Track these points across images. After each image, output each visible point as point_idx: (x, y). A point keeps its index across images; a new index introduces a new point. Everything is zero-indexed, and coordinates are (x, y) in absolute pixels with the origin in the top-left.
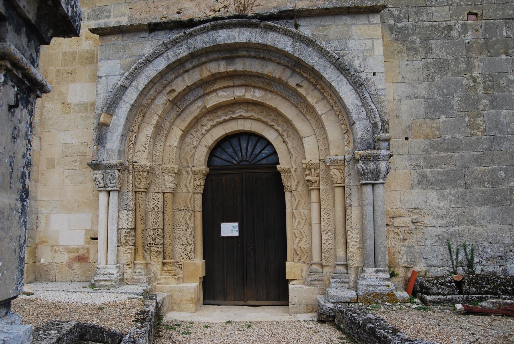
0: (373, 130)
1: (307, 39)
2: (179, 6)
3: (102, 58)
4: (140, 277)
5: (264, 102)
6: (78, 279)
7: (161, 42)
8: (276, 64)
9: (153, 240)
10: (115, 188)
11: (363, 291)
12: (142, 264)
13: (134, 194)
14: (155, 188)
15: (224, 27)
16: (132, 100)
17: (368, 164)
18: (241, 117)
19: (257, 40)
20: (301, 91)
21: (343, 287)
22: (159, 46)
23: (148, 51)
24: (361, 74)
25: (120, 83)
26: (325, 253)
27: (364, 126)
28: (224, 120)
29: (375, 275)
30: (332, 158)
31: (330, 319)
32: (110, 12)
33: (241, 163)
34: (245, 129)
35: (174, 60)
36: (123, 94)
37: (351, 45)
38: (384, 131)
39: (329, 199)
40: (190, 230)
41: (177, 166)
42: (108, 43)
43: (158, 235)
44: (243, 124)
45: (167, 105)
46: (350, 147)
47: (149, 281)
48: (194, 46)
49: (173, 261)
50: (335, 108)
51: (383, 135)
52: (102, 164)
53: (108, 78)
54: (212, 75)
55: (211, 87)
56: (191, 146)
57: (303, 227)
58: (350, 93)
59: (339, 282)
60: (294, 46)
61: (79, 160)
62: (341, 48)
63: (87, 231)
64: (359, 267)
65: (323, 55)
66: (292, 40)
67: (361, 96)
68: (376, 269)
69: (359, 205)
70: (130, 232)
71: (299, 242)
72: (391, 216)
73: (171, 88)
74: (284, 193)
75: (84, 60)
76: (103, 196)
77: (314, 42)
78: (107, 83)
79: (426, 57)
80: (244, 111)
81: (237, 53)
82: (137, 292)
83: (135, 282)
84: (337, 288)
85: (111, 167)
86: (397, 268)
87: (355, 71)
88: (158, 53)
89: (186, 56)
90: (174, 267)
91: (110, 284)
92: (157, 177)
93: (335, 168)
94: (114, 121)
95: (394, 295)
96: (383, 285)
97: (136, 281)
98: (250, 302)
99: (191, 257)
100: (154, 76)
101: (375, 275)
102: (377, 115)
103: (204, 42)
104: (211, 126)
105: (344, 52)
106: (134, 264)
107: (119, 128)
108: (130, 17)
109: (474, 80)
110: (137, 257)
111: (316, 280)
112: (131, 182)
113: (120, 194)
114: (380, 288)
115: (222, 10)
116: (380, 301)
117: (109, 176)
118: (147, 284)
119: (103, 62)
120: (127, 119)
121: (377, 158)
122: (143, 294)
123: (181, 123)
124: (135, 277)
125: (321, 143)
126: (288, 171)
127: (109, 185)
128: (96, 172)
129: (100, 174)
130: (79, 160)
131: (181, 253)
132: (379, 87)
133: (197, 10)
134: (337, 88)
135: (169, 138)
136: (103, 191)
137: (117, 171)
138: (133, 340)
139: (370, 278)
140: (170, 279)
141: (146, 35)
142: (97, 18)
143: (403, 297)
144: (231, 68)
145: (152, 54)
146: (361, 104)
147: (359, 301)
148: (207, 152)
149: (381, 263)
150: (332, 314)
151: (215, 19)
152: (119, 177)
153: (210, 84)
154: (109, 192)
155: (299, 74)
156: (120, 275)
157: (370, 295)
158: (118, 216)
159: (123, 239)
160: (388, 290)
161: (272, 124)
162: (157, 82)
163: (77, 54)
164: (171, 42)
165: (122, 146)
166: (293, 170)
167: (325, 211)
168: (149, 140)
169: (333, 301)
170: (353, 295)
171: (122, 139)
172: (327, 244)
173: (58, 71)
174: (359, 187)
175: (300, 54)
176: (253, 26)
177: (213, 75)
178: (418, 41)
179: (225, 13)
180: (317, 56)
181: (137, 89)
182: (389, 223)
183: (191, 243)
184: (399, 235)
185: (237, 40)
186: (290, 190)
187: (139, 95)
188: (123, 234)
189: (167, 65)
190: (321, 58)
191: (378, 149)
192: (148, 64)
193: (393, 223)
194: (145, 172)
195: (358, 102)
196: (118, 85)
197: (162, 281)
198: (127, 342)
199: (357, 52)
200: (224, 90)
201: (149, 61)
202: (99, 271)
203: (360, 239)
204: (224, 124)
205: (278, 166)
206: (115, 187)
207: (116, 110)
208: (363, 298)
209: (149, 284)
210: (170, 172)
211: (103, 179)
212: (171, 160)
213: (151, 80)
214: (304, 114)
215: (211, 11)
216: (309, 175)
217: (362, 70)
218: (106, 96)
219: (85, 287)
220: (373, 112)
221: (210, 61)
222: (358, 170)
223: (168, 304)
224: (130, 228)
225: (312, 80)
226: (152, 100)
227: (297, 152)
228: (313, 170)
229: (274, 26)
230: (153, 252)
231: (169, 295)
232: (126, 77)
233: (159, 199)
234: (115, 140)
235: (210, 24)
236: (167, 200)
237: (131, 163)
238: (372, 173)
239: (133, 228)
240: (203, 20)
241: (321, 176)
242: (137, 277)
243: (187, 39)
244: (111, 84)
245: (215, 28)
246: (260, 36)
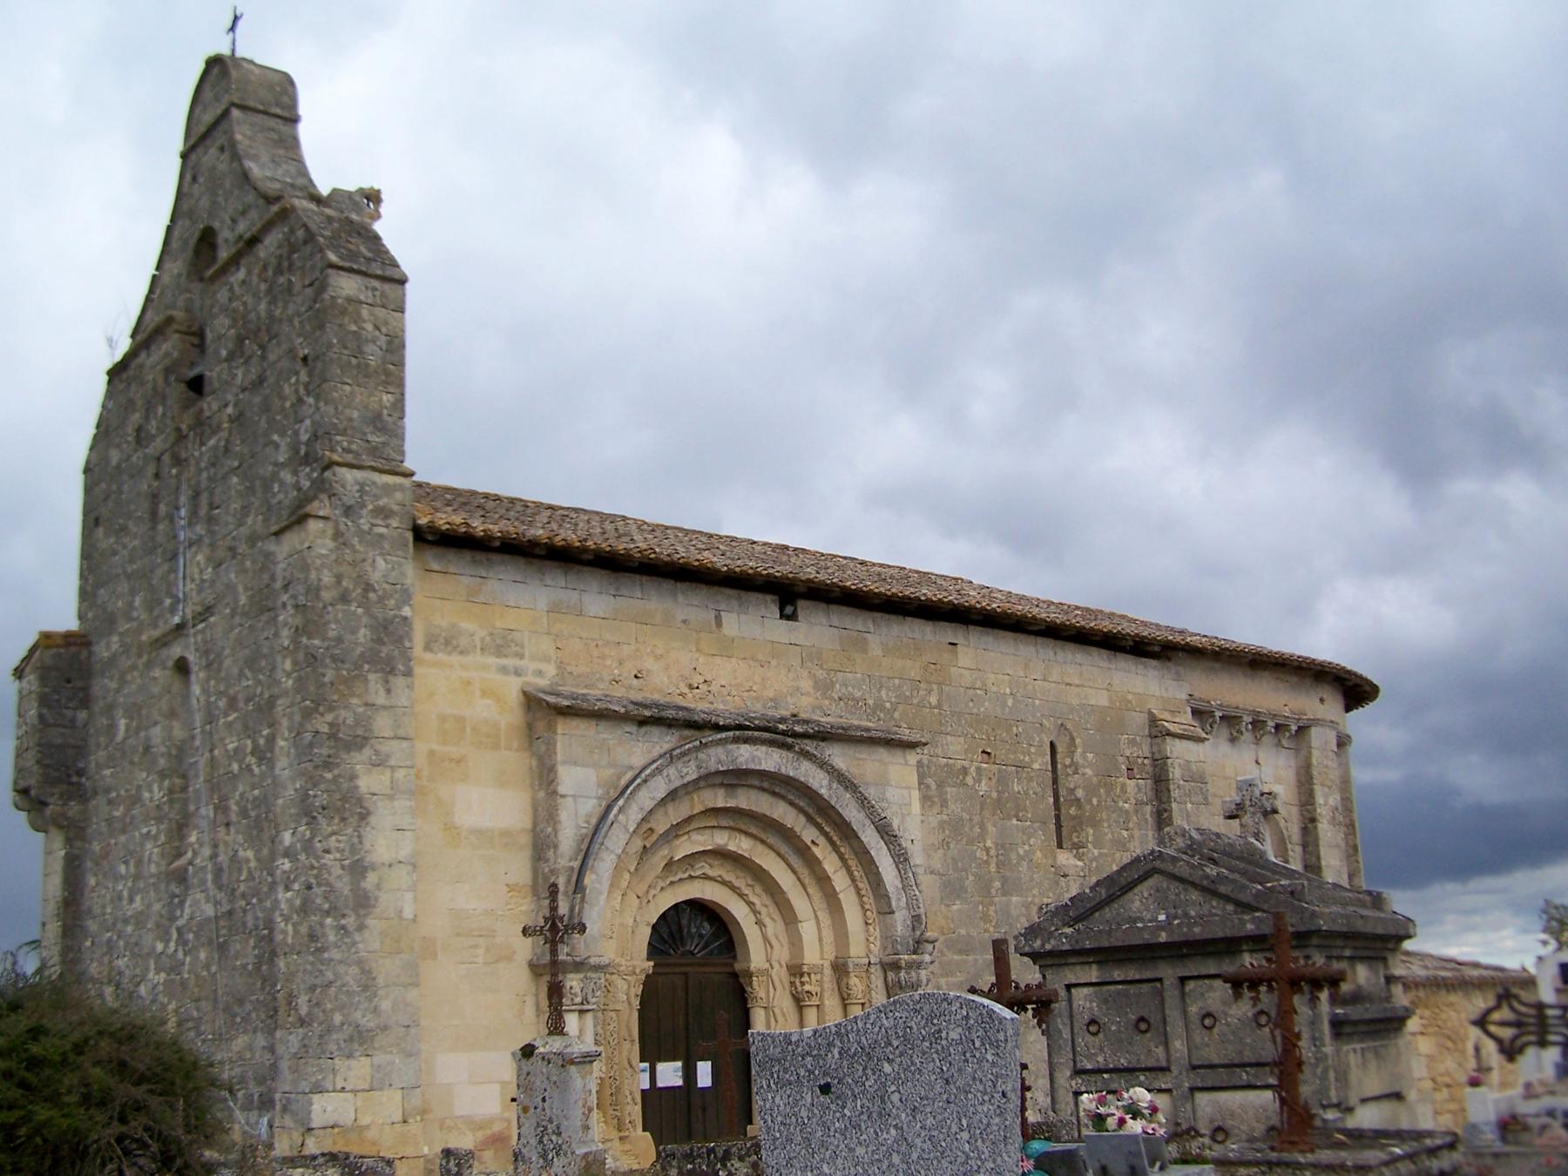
20: (816, 851)
78: (576, 810)
79: (941, 813)
103: (720, 762)
109: (987, 850)
141: (633, 728)
144: (731, 804)
173: (432, 753)
178: (934, 786)
184: (1477, 1049)
245: (736, 740)
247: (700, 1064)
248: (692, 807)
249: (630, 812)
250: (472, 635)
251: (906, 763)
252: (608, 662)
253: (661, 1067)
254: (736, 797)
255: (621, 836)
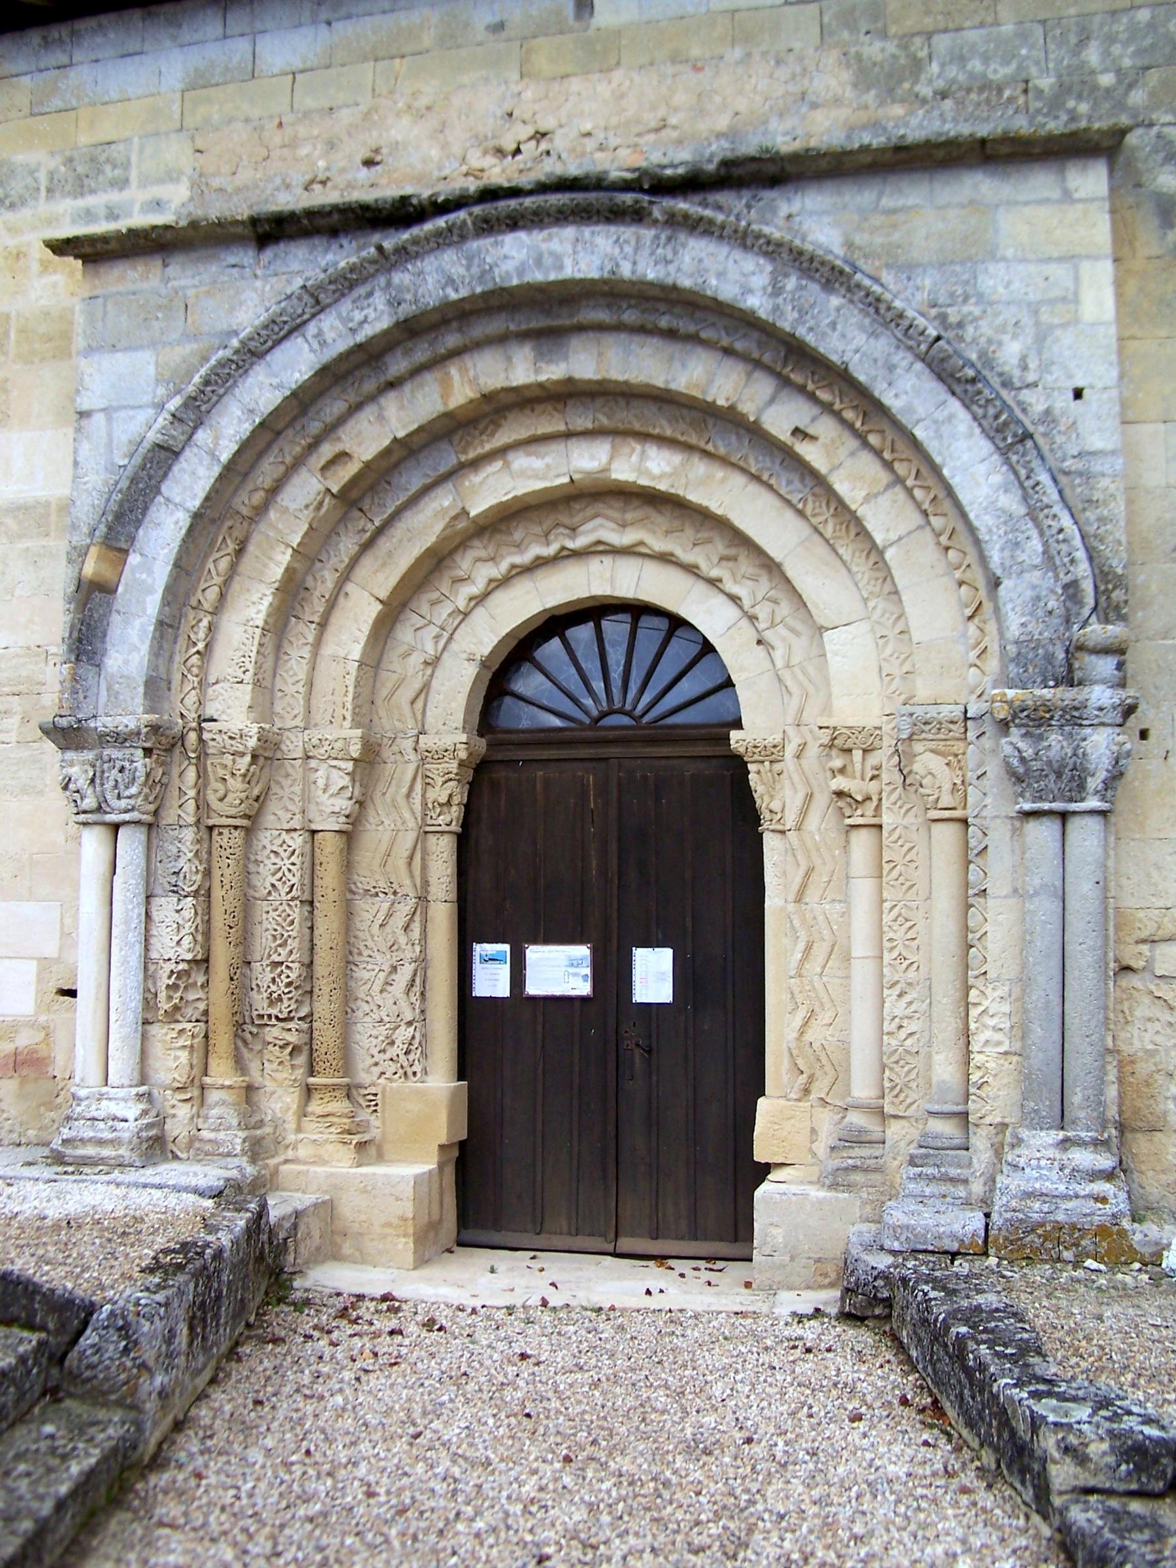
0: (1068, 610)
1: (823, 263)
2: (372, 138)
3: (94, 345)
4: (221, 1135)
5: (681, 493)
6: (15, 1136)
7: (299, 282)
8: (719, 355)
9: (271, 1003)
10: (134, 816)
11: (1008, 1215)
12: (230, 1087)
13: (206, 836)
14: (280, 813)
15: (521, 223)
16: (195, 497)
17: (1041, 738)
18: (601, 548)
19: (640, 268)
20: (808, 451)
21: (944, 1196)
22: (289, 297)
23: (251, 314)
24: (1025, 395)
25: (152, 436)
26: (891, 1069)
27: (1034, 594)
28: (538, 558)
29: (1058, 1156)
30: (919, 711)
31: (877, 1311)
32: (127, 166)
33: (602, 723)
34: (618, 593)
35: (342, 346)
36: (165, 475)
37: (991, 283)
38: (1106, 615)
39: (913, 865)
40: (406, 972)
41: (359, 732)
42: (114, 289)
43: (289, 984)
44: (608, 575)
45: (323, 510)
46: (987, 669)
47: (256, 1150)
48: (415, 295)
49: (346, 1080)
50: (937, 522)
51: (1098, 632)
52: (88, 729)
53: (115, 416)
54: (484, 396)
55: (484, 437)
56: (416, 659)
57: (824, 967)
58: (982, 468)
59: (931, 1179)
60: (776, 290)
61: (19, 709)
62: (952, 295)
63: (45, 963)
64: (1005, 1125)
65: (886, 324)
66: (769, 268)
67: (1023, 477)
68: (1061, 1135)
69: (1015, 891)
70: (187, 973)
71: (806, 1023)
72: (1144, 934)
73: (338, 448)
74: (759, 838)
75: (37, 346)
76: (93, 843)
77: (850, 277)
80: (612, 525)
81: (571, 316)
82: (202, 1183)
83: (198, 1149)
84: (922, 1200)
85: (120, 739)
86: (1158, 1134)
87: (1004, 385)
88: (285, 322)
89: (386, 333)
90: (346, 1103)
91: (114, 1153)
92: (288, 775)
93: (932, 751)
94: (133, 571)
95: (1122, 1233)
96: (1082, 1193)
97: (208, 1147)
98: (625, 1244)
99: (410, 1071)
100: (271, 408)
101: (1058, 1156)
102: (1081, 554)
103: (450, 281)
104: (491, 581)
105: (965, 309)
106: (202, 1088)
107: (149, 599)
108: (199, 185)
110: (213, 1062)
111: (855, 1168)
112: (192, 793)
113: (154, 834)
114: (1070, 1205)
115: (528, 148)
116: (1067, 1255)
117: (115, 772)
118: (244, 1161)
119: (96, 357)
120: (177, 565)
121: (1074, 717)
122: (221, 1192)
123: (375, 573)
124: (206, 1134)
125: (888, 651)
126: (773, 754)
127: (115, 803)
128: (70, 755)
129: (83, 763)
130: (19, 709)
131: (375, 1051)
132: (1097, 442)
133: (435, 153)
134: (932, 447)
135: (331, 629)
136: (95, 823)
137: (140, 753)
138: (121, 1323)
139: (1039, 1167)
140: (330, 1147)
141: (245, 256)
142: (81, 188)
143: (1157, 1244)
144: (553, 372)
145: (266, 327)
146: (1023, 510)
147: (992, 1251)
148: (478, 677)
149: (1082, 1114)
150: (885, 1294)
151: (490, 194)
152: (148, 775)
153: (481, 426)
154: (116, 827)
155: (802, 389)
156: (150, 1126)
157: (1033, 1230)
158: (148, 915)
159: (162, 996)
160: (1102, 1214)
161: (714, 573)
162: (286, 427)
163: (13, 322)
164: (330, 282)
165: (161, 661)
166: (790, 750)
167: (896, 911)
168: (257, 637)
169: (896, 1246)
170: (969, 1229)
171: (162, 637)
172: (903, 1034)
174: (1017, 824)
175: (800, 321)
176: (628, 219)
177: (487, 398)
179: (537, 160)
180: (861, 328)
181: (212, 454)
182: (1133, 963)
183: (410, 1018)
185: (569, 271)
186: (780, 827)
187: (221, 478)
188: (164, 981)
189: (318, 366)
190: (874, 335)
191: (1080, 684)
192: (252, 364)
193: (1150, 961)
194: (243, 754)
195: (1012, 503)
196: (146, 445)
197: (302, 1152)
198: (105, 1328)
199: (1013, 309)
200: (533, 448)
201: (253, 353)
202: (79, 1109)
203: (1014, 1019)
204: (540, 574)
205: (734, 735)
206: (133, 809)
207: (141, 532)
208: (1006, 1239)
209: (253, 1160)
210: (334, 754)
211: (93, 781)
212: (340, 712)
213: (261, 424)
214: (827, 541)
215: (485, 153)
216: (842, 771)
217: (1031, 377)
218: (106, 483)
219: (30, 1164)
220: (1064, 541)
221: (478, 345)
222: (1007, 764)
223: (316, 1234)
224: (189, 956)
225: (849, 415)
226: (267, 491)
227: (806, 683)
228: (857, 755)
229: (701, 219)
230: (270, 1047)
231: (324, 1203)
232: (173, 415)
233: (293, 853)
234: (135, 639)
235: (470, 214)
236: (323, 860)
237: (194, 725)
238: (1059, 775)
239: (199, 957)
240: (447, 201)
241: (885, 777)
242: (212, 1136)
243: (389, 271)
244: (124, 438)
245: (487, 227)
246: (652, 254)
247: (641, 955)
248: (445, 396)
249: (224, 421)
250: (32, 172)
251: (1067, 197)
252: (304, 151)
253: (535, 954)
254: (566, 359)
255: (202, 471)
